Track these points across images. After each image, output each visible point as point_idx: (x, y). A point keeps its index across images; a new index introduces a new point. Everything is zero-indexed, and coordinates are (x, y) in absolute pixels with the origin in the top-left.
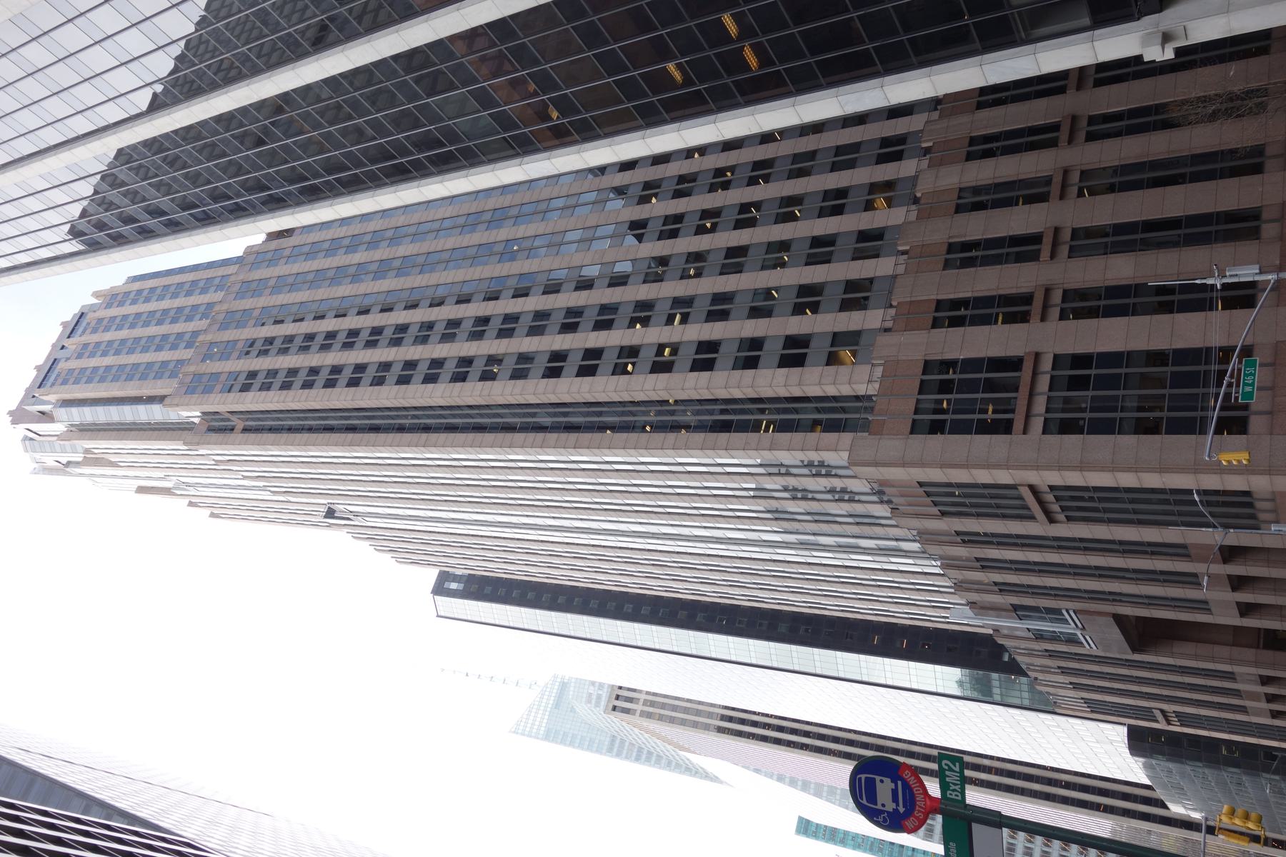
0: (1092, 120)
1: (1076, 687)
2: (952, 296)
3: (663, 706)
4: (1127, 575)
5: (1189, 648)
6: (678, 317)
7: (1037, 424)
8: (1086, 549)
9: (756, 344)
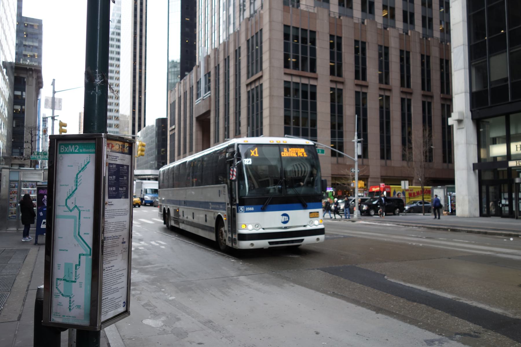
0: (409, 100)
1: (180, 98)
2: (343, 43)
5: (200, 137)
7: (288, 79)
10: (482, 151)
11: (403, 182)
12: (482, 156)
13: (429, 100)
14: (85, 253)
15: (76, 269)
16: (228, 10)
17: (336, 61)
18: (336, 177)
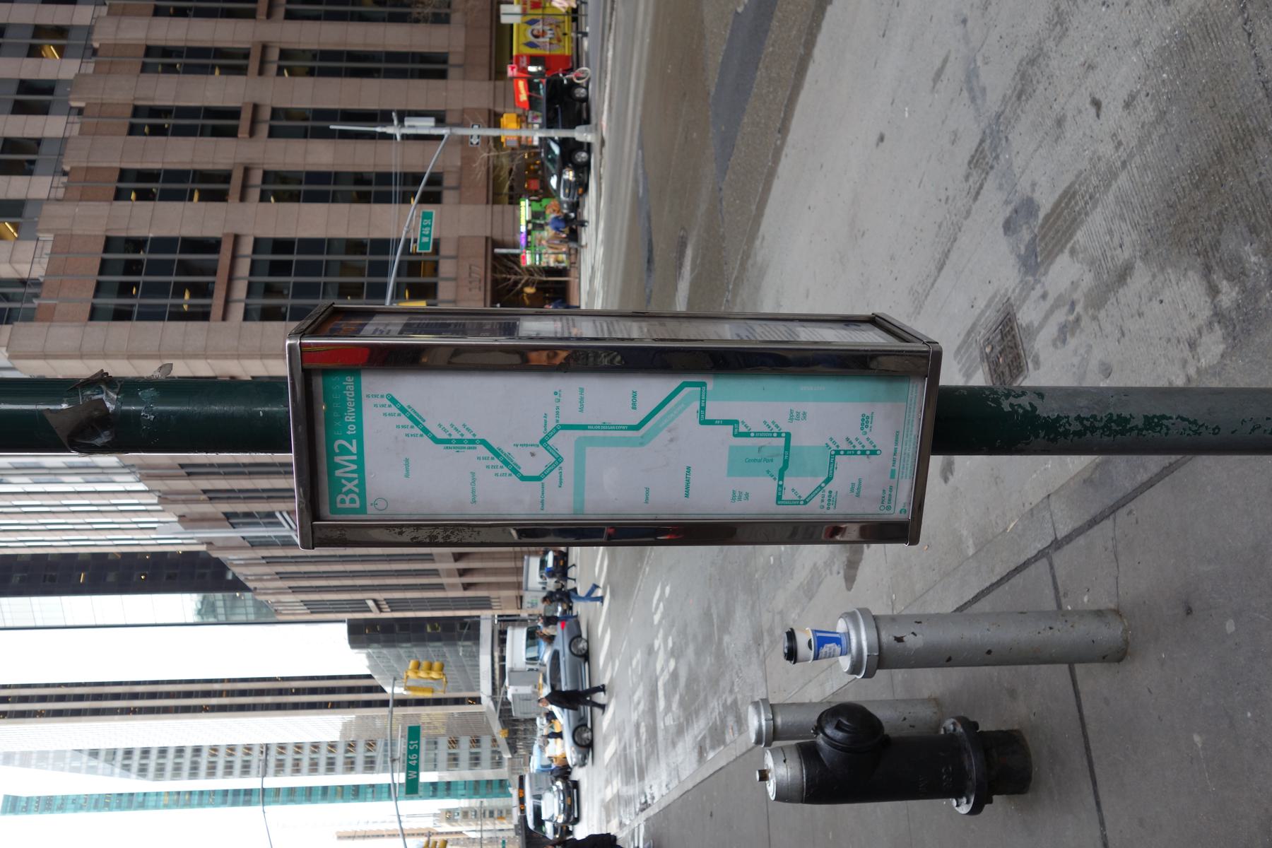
1: (295, 590)
2: (138, 166)
7: (238, 310)
11: (505, 20)
14: (697, 405)
15: (747, 435)
17: (188, 186)
18: (494, 194)
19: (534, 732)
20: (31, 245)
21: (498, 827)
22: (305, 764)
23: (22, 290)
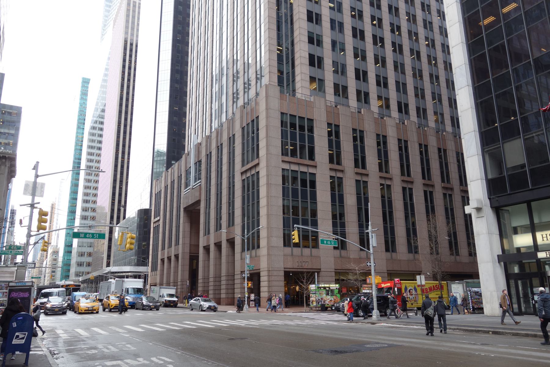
0: (411, 189)
1: (166, 187)
2: (341, 132)
3: (134, 11)
4: (207, 209)
6: (332, 5)
7: (286, 166)
8: (217, 194)
9: (319, 43)
10: (505, 241)
11: (418, 277)
12: (506, 247)
13: (431, 190)
16: (220, 98)
19: (91, 292)
20: (309, 94)
21: (46, 275)
22: (88, 191)
23: (291, 89)
